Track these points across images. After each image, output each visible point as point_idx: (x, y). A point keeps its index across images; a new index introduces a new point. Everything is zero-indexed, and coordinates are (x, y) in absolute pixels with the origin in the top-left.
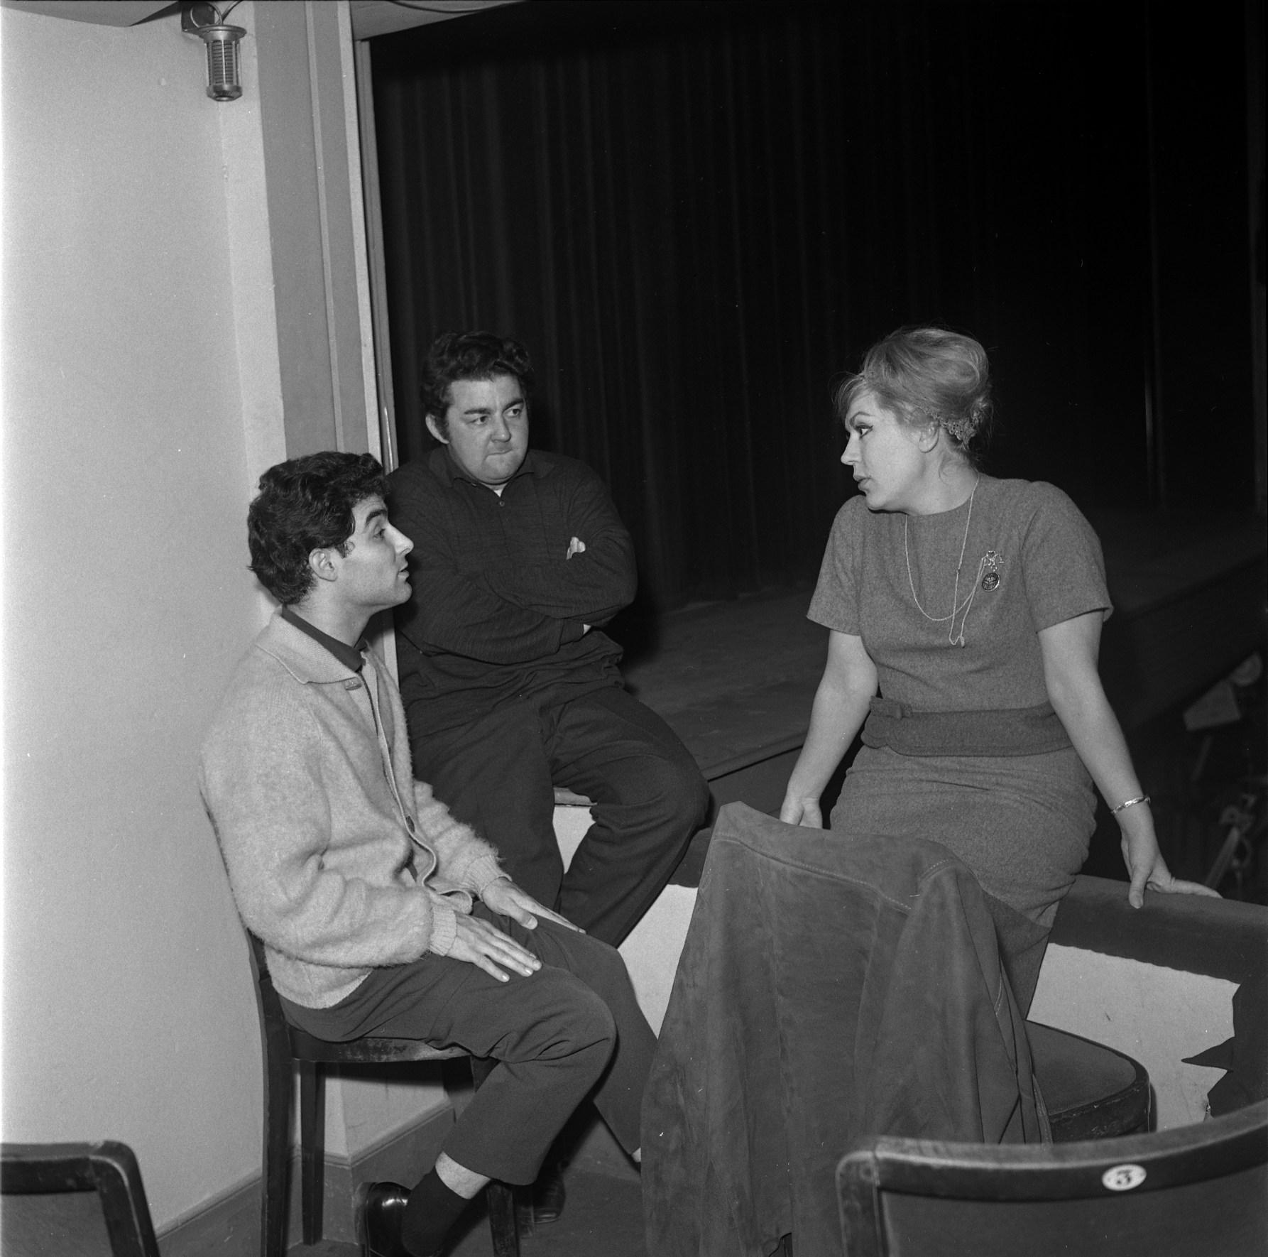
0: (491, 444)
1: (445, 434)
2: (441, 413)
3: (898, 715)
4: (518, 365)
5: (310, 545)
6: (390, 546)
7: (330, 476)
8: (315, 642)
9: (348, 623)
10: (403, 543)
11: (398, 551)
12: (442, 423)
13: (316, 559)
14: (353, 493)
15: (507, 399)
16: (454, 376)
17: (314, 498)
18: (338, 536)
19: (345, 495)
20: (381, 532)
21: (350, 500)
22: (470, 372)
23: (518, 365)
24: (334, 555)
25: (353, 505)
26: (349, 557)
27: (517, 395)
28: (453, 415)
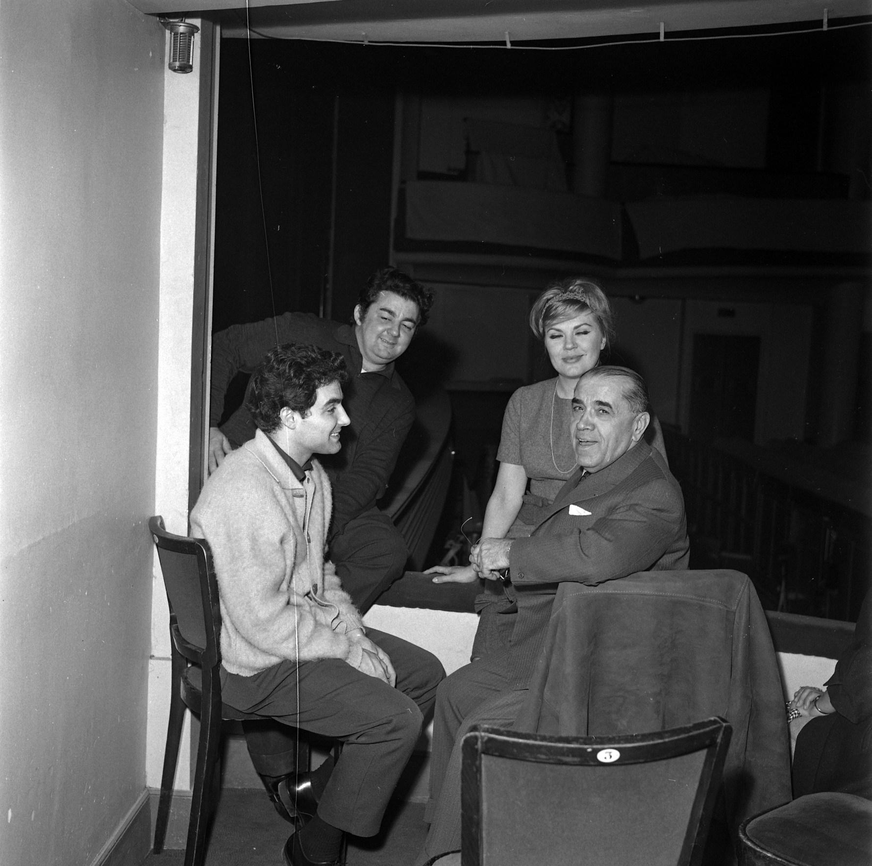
0: (385, 333)
1: (362, 319)
2: (366, 306)
3: (541, 505)
4: (424, 302)
5: (284, 404)
6: (336, 419)
7: (308, 364)
8: (283, 461)
9: (301, 454)
10: (344, 419)
11: (339, 422)
12: (364, 311)
13: (285, 413)
14: (319, 379)
15: (408, 316)
16: (388, 288)
17: (295, 376)
18: (303, 406)
19: (313, 380)
20: (333, 410)
21: (317, 383)
22: (396, 289)
23: (424, 302)
24: (297, 416)
25: (317, 387)
26: (306, 420)
27: (415, 318)
28: (374, 310)
